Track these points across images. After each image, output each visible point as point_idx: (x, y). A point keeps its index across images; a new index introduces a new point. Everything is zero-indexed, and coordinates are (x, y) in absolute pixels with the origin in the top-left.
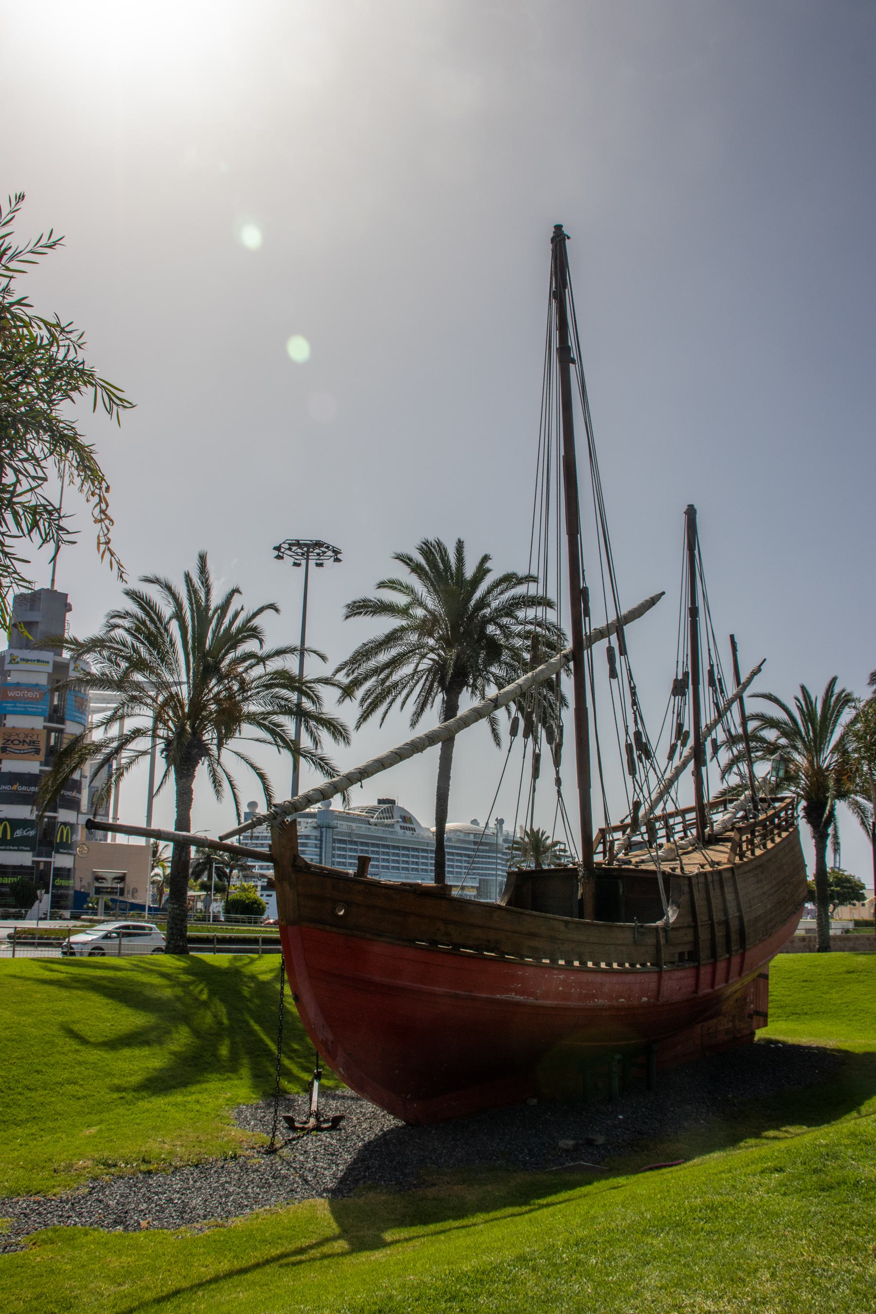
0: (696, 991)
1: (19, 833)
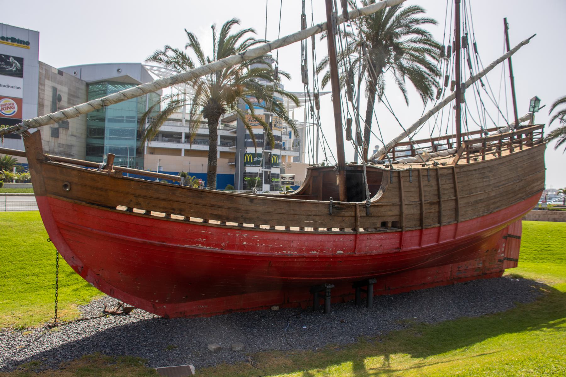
0: (400, 248)
1: (256, 159)
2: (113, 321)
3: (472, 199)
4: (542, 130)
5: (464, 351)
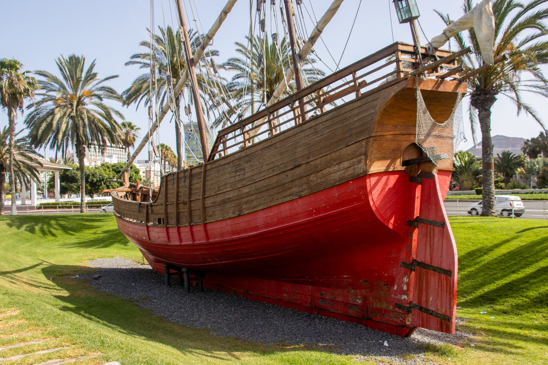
3: (219, 198)
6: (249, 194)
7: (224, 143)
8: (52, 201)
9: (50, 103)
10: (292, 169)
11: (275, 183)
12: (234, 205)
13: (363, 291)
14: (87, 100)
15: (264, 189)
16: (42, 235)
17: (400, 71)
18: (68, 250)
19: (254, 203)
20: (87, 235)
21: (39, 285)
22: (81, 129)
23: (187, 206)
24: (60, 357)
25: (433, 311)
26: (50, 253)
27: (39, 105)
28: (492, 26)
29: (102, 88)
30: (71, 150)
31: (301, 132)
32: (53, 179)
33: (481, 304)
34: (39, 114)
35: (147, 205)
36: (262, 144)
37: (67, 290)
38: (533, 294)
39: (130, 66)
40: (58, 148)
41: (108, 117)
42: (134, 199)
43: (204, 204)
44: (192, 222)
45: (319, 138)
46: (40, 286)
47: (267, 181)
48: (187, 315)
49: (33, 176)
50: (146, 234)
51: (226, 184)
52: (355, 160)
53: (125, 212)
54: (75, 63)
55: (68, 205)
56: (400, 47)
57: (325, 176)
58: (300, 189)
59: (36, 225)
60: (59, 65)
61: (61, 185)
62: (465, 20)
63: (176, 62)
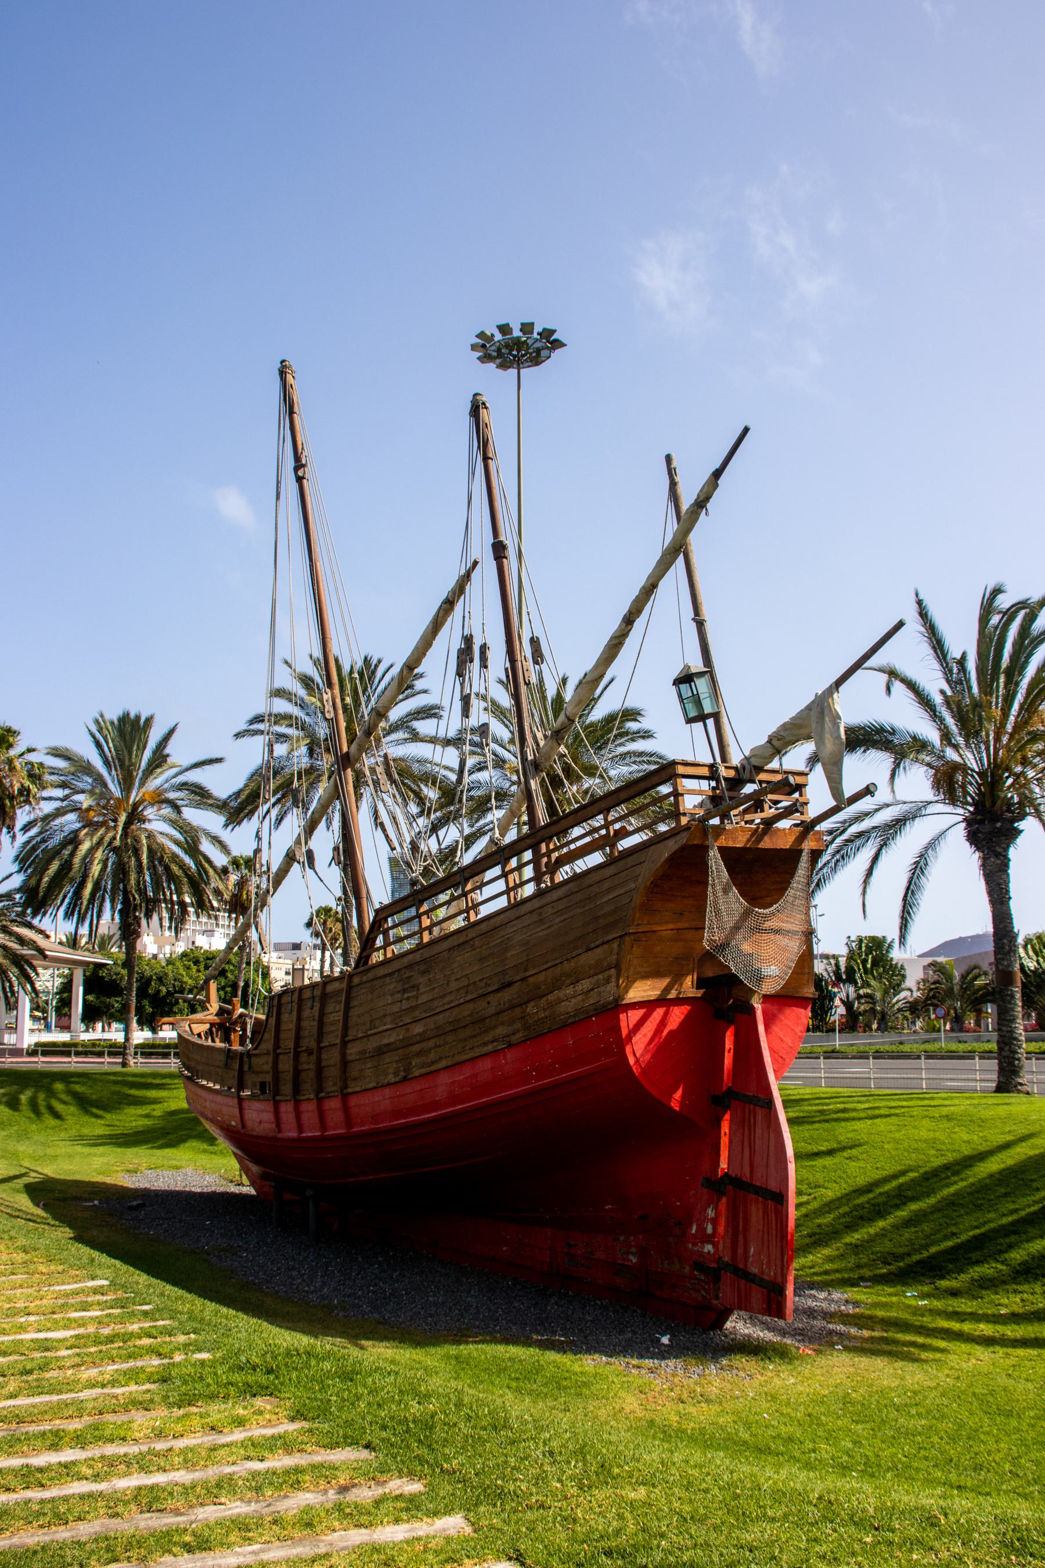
2: (233, 1189)
3: (373, 1044)
4: (271, 751)
5: (397, 1347)
6: (423, 1038)
7: (385, 933)
8: (64, 1037)
9: (72, 817)
10: (497, 991)
11: (469, 1015)
12: (396, 1058)
13: (641, 1237)
14: (150, 812)
15: (450, 1028)
16: (33, 1116)
17: (681, 814)
18: (87, 1150)
19: (432, 1056)
20: (132, 1118)
21: (17, 1214)
22: (133, 877)
23: (313, 1058)
24: (28, 1273)
25: (755, 1275)
26: (45, 1155)
27: (49, 823)
28: (839, 736)
29: (185, 784)
30: (108, 921)
31: (518, 918)
32: (67, 987)
33: (913, 1278)
34: (46, 841)
35: (242, 1054)
36: (450, 939)
37: (71, 1228)
38: (1017, 1256)
39: (247, 740)
40: (81, 920)
41: (192, 848)
42: (226, 1039)
43: (343, 1055)
44: (322, 1092)
45: (545, 932)
46: (18, 1217)
47: (456, 1011)
48: (299, 1281)
49: (23, 980)
50: (236, 1111)
51: (385, 1016)
52: (600, 976)
53: (200, 1068)
54: (129, 731)
55: (97, 1049)
56: (681, 770)
57: (551, 1006)
58: (511, 1029)
59: (21, 1092)
60: (93, 736)
61: (85, 1000)
62: (799, 722)
63: (337, 735)
